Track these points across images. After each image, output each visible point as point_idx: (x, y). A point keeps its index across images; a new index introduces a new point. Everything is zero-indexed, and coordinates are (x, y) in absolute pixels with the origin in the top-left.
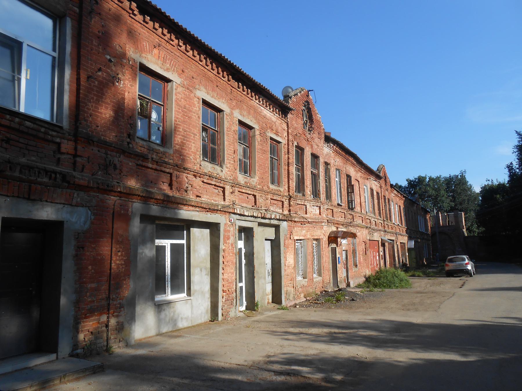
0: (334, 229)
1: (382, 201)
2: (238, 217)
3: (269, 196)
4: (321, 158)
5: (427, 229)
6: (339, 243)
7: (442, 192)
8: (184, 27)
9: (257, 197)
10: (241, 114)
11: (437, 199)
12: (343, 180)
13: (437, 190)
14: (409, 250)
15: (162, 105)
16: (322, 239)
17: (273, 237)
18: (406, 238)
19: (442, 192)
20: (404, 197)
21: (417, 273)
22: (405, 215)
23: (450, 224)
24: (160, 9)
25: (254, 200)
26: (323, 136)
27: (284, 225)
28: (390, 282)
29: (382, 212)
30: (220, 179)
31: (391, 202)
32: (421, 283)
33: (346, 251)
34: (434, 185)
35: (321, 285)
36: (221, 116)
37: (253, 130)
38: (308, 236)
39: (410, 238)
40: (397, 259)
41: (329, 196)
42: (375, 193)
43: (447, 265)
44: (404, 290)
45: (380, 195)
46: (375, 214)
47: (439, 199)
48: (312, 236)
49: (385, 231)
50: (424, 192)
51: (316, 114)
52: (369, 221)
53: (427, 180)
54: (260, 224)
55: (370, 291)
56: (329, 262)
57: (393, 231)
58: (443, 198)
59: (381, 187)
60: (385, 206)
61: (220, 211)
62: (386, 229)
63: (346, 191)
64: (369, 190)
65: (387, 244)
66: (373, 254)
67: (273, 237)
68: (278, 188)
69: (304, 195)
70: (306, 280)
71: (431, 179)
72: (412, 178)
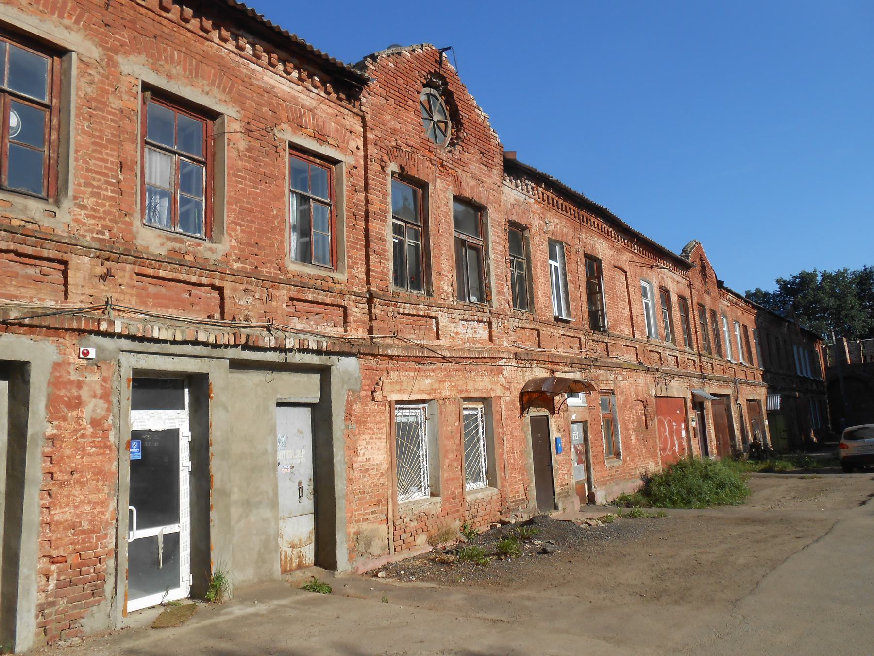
0: (541, 373)
1: (694, 316)
2: (125, 344)
3: (283, 293)
4: (491, 210)
5: (816, 370)
6: (557, 406)
7: (851, 300)
8: (274, 24)
9: (227, 292)
10: (154, 70)
11: (839, 313)
12: (574, 265)
13: (841, 297)
14: (771, 414)
15: (203, 163)
16: (499, 397)
17: (315, 397)
18: (763, 391)
19: (851, 300)
20: (754, 307)
21: (779, 465)
22: (760, 344)
23: (868, 361)
24: (287, 32)
25: (218, 302)
26: (498, 160)
27: (346, 367)
28: (689, 491)
29: (693, 336)
30: (202, 267)
31: (719, 317)
32: (778, 493)
33: (585, 423)
34: (833, 289)
35: (496, 507)
36: (65, 65)
37: (218, 121)
38: (446, 393)
39: (772, 390)
40: (737, 433)
41: (523, 297)
42: (674, 298)
43: (844, 446)
44: (711, 512)
45: (689, 301)
46: (674, 341)
47: (843, 313)
48: (461, 391)
49: (703, 377)
50: (811, 303)
51: (470, 109)
52: (656, 356)
53: (819, 278)
54: (237, 365)
55: (632, 516)
56: (523, 453)
57: (726, 376)
58: (853, 312)
59: (690, 286)
60: (704, 325)
61: (21, 325)
62: (708, 372)
63: (583, 289)
64: (656, 291)
65: (708, 405)
66: (670, 426)
67: (315, 397)
68: (323, 273)
69: (429, 294)
70: (438, 499)
71: (825, 276)
72: (787, 277)
